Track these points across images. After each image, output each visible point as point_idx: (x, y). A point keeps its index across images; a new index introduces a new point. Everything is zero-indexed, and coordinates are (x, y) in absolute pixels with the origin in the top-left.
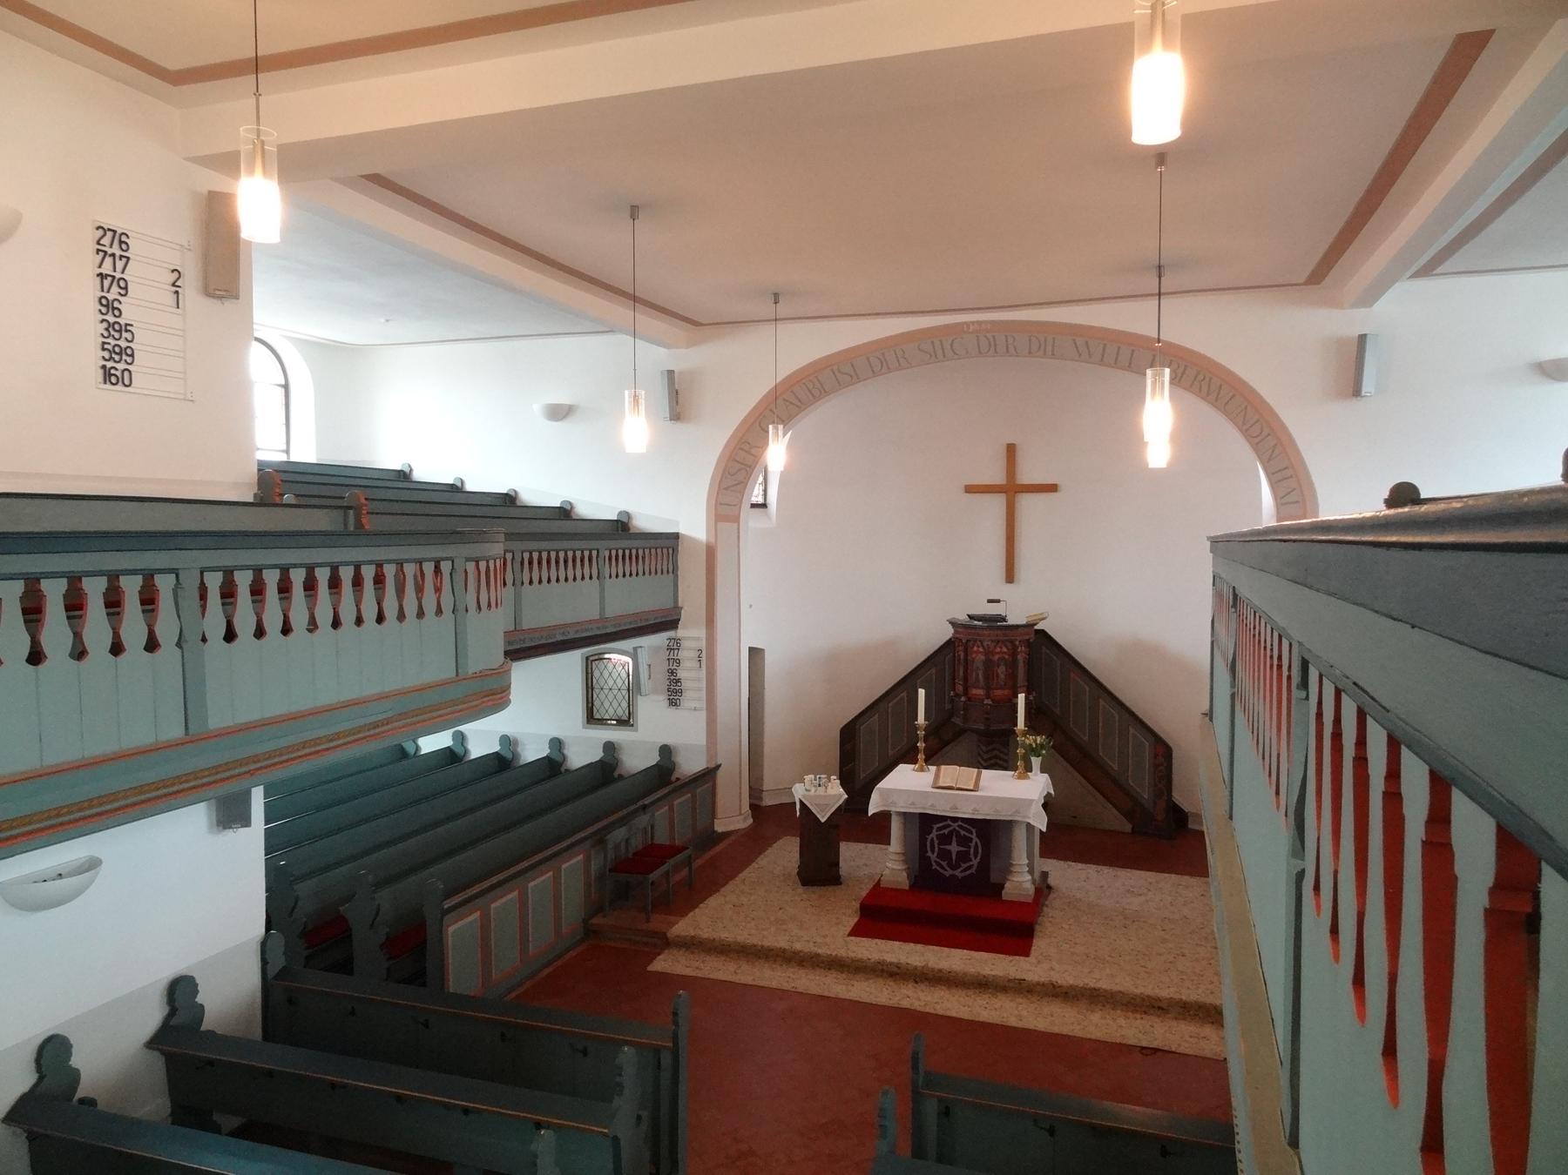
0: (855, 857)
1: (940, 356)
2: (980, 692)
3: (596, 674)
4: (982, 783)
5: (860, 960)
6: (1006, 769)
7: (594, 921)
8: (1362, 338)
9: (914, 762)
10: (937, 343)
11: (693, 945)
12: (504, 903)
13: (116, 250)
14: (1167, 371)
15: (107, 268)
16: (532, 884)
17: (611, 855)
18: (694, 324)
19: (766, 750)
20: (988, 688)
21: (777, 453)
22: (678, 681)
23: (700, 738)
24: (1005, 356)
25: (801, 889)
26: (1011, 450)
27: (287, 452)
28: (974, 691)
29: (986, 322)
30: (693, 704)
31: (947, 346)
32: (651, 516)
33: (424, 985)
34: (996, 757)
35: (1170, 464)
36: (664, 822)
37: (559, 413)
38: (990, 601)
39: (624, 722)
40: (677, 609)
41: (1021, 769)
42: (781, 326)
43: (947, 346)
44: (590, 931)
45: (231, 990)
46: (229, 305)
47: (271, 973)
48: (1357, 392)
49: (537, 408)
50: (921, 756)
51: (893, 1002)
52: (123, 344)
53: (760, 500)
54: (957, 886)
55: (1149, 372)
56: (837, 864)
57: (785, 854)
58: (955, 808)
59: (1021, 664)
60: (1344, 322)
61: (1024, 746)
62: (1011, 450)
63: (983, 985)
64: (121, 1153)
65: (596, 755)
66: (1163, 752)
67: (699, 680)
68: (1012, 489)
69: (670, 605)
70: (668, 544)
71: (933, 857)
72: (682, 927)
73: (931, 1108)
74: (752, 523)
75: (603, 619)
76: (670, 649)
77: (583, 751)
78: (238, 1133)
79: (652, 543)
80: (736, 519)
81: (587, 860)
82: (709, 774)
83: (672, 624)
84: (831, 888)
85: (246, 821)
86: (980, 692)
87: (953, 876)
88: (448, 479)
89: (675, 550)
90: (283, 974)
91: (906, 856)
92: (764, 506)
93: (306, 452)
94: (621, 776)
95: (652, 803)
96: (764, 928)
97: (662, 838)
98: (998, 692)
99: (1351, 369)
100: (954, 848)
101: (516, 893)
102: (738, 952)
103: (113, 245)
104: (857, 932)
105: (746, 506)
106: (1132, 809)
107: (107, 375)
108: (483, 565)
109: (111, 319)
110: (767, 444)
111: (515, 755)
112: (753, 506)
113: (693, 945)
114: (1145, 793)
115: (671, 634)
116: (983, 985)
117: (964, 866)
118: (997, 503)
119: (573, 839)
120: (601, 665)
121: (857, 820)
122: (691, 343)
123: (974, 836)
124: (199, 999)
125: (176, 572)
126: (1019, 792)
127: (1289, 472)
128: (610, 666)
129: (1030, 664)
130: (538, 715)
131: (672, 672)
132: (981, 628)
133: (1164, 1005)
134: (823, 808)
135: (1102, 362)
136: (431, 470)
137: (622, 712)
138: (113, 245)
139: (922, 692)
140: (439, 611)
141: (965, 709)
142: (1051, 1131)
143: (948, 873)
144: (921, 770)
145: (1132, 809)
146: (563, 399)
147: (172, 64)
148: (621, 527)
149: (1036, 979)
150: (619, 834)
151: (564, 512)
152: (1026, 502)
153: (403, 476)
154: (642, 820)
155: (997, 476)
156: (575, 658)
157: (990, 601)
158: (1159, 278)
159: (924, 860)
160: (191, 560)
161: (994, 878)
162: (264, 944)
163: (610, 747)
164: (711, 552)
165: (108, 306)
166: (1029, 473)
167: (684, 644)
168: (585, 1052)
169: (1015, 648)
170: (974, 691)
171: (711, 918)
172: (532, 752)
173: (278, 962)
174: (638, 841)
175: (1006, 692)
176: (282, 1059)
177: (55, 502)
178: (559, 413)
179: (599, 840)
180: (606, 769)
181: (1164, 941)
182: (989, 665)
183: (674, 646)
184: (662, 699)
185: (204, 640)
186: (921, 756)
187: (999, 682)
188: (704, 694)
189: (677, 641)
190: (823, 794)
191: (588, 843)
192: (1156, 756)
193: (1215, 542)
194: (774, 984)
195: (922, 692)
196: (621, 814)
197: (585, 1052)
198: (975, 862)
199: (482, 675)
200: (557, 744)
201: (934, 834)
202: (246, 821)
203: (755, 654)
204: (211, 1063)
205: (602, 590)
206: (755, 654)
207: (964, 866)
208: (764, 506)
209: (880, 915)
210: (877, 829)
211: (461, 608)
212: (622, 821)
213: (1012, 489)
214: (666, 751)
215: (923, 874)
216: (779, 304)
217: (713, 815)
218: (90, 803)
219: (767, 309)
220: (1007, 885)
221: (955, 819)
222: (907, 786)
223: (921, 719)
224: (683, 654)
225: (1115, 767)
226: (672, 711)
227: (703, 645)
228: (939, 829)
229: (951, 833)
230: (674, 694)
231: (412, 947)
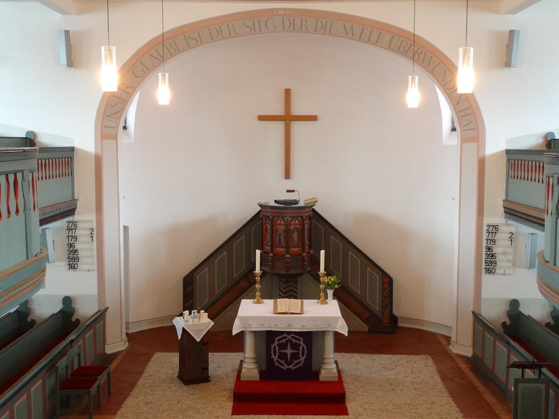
0: (221, 363)
2: (282, 250)
8: (512, 32)
9: (253, 297)
19: (107, 290)
20: (288, 247)
22: (76, 251)
23: (94, 291)
25: (185, 388)
26: (288, 92)
29: (289, 9)
30: (86, 267)
34: (291, 290)
35: (172, 102)
38: (288, 191)
41: (322, 298)
48: (508, 64)
50: (258, 294)
56: (207, 368)
57: (167, 363)
58: (290, 326)
59: (306, 231)
60: (503, 22)
61: (324, 283)
62: (288, 92)
66: (387, 281)
67: (91, 250)
68: (288, 118)
70: (63, 159)
71: (276, 358)
74: (124, 140)
76: (69, 229)
80: (115, 138)
81: (44, 384)
83: (71, 212)
84: (204, 385)
86: (282, 250)
87: (288, 369)
89: (514, 33)
91: (257, 360)
98: (293, 250)
100: (289, 351)
106: (370, 318)
110: (407, 88)
115: (70, 219)
117: (296, 362)
121: (224, 339)
122: (79, 13)
123: (302, 343)
126: (323, 313)
127: (468, 112)
129: (310, 230)
131: (71, 245)
132: (282, 208)
135: (360, 39)
141: (272, 262)
143: (285, 367)
145: (370, 318)
150: (62, 363)
152: (296, 126)
155: (279, 111)
157: (288, 191)
159: (270, 361)
161: (314, 369)
164: (98, 160)
166: (296, 110)
169: (303, 220)
181: (419, 396)
182: (288, 232)
183: (72, 227)
184: (63, 265)
186: (258, 294)
187: (288, 244)
189: (74, 223)
192: (383, 283)
193: (260, 205)
198: (302, 359)
201: (276, 343)
203: (126, 228)
206: (126, 228)
207: (296, 362)
210: (236, 343)
213: (288, 118)
214: (67, 301)
215: (269, 371)
220: (323, 371)
221: (289, 333)
222: (255, 313)
223: (258, 270)
225: (359, 292)
226: (72, 273)
227: (94, 226)
228: (279, 340)
229: (287, 342)
230: (73, 260)
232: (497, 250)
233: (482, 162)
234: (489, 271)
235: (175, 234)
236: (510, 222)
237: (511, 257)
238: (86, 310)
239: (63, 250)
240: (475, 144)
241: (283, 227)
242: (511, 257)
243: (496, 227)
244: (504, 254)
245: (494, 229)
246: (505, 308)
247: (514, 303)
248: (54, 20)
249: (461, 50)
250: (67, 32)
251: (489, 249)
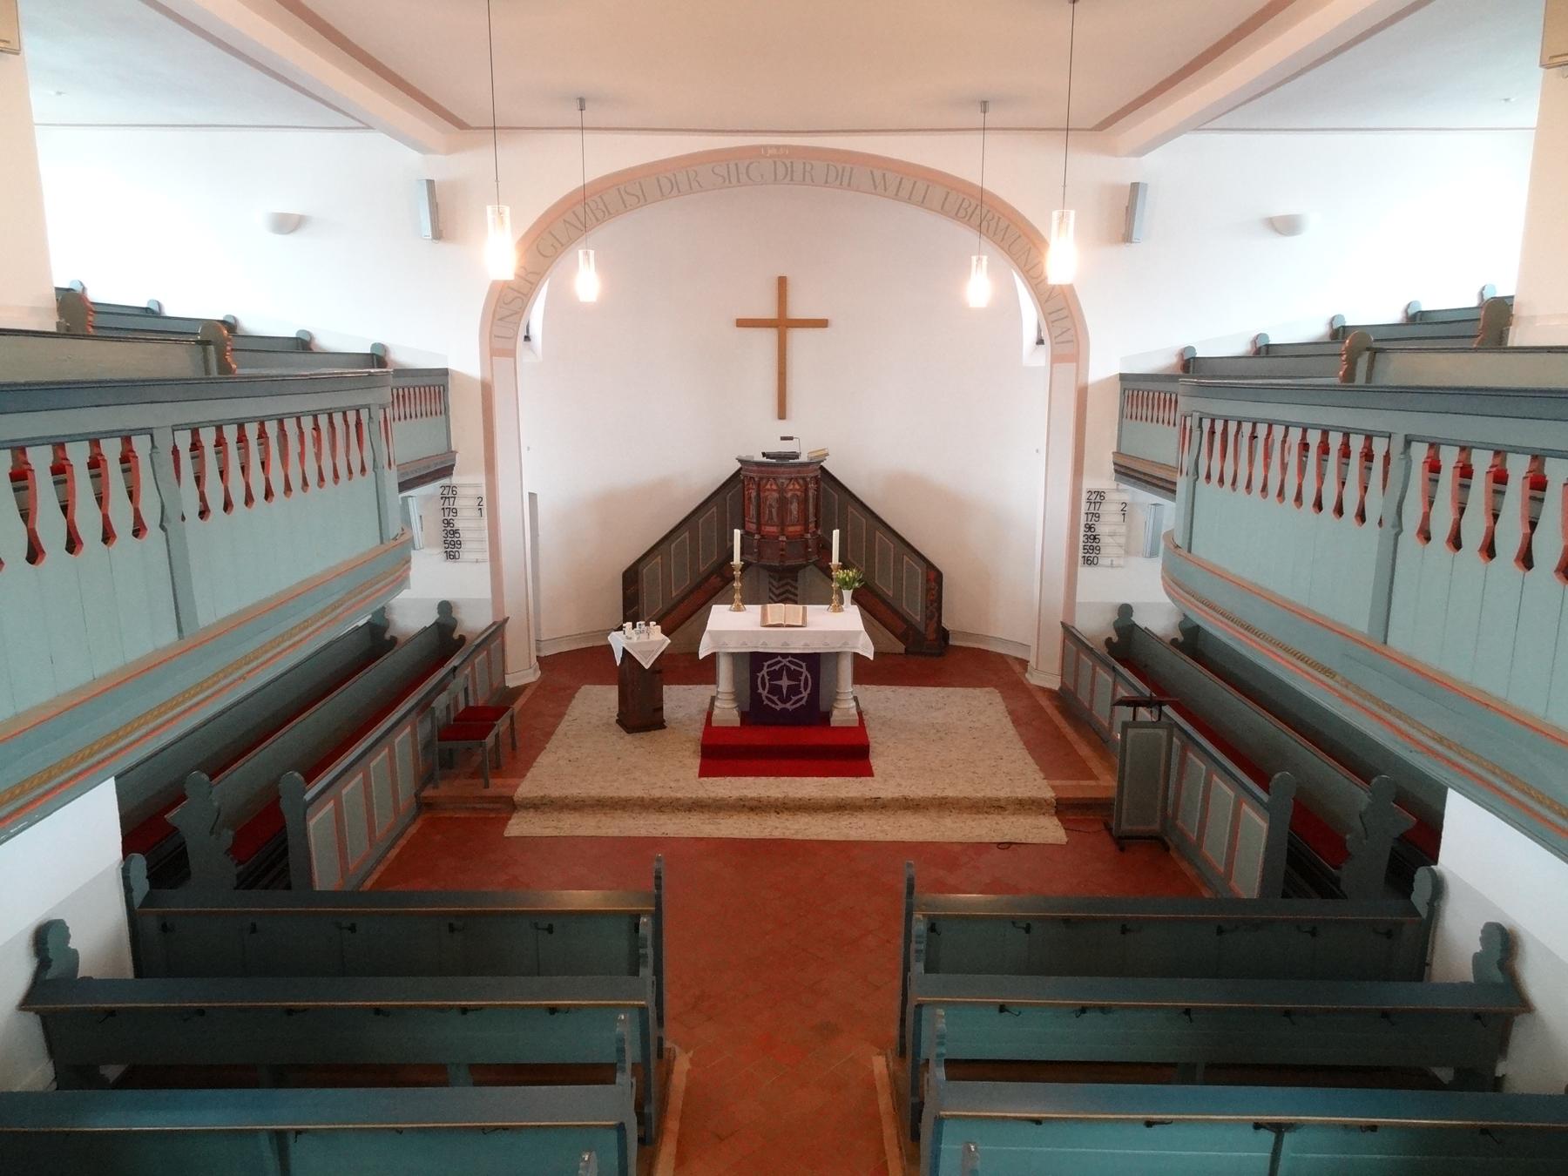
0: (682, 702)
1: (734, 180)
2: (774, 529)
4: (809, 619)
5: (722, 799)
6: (796, 603)
7: (424, 794)
8: (1135, 187)
10: (732, 167)
11: (541, 805)
14: (1072, 213)
22: (455, 532)
23: (484, 591)
24: (789, 186)
25: (628, 737)
26: (782, 282)
28: (768, 529)
29: (785, 147)
30: (473, 556)
31: (742, 170)
32: (413, 348)
33: (288, 887)
36: (460, 687)
37: (288, 224)
38: (783, 439)
40: (451, 453)
42: (989, 136)
43: (742, 170)
44: (423, 805)
45: (99, 931)
47: (138, 897)
48: (1127, 238)
50: (737, 596)
51: (766, 834)
54: (788, 720)
57: (599, 701)
60: (1126, 169)
61: (838, 580)
62: (782, 282)
63: (841, 807)
64: (68, 1134)
66: (934, 577)
68: (782, 324)
70: (431, 387)
71: (765, 693)
72: (526, 789)
73: (919, 927)
74: (527, 358)
76: (444, 498)
78: (123, 1083)
80: (512, 353)
81: (414, 733)
82: (498, 629)
83: (446, 471)
86: (774, 529)
88: (142, 302)
90: (148, 901)
91: (736, 696)
96: (595, 782)
98: (791, 529)
99: (1125, 216)
100: (785, 683)
102: (592, 806)
104: (705, 772)
113: (541, 805)
114: (917, 615)
116: (841, 807)
117: (794, 699)
122: (451, 150)
123: (804, 670)
124: (72, 945)
125: (148, 431)
126: (836, 624)
129: (817, 499)
133: (1003, 804)
134: (646, 654)
135: (896, 197)
142: (1028, 929)
144: (738, 609)
146: (293, 208)
149: (890, 796)
150: (441, 701)
151: (302, 345)
152: (797, 337)
155: (770, 312)
157: (783, 439)
158: (984, 112)
159: (755, 697)
161: (823, 708)
164: (487, 390)
166: (796, 311)
168: (550, 930)
169: (806, 484)
170: (768, 529)
171: (539, 779)
174: (441, 704)
175: (798, 528)
176: (157, 996)
177: (1545, 356)
178: (288, 224)
182: (783, 502)
183: (449, 494)
184: (437, 553)
185: (183, 518)
186: (737, 596)
187: (783, 520)
188: (486, 545)
189: (452, 488)
190: (644, 641)
191: (414, 713)
192: (928, 580)
194: (643, 833)
197: (550, 930)
198: (805, 694)
203: (532, 496)
204: (111, 1013)
206: (532, 496)
207: (794, 699)
209: (720, 754)
210: (704, 671)
213: (782, 324)
214: (445, 607)
215: (754, 712)
216: (583, 111)
217: (504, 672)
219: (573, 116)
220: (835, 712)
221: (785, 656)
222: (732, 625)
223: (737, 560)
224: (459, 503)
226: (450, 564)
227: (483, 492)
230: (452, 545)
231: (267, 846)
232: (1102, 529)
233: (1082, 394)
234: (1088, 561)
235: (608, 505)
236: (1123, 486)
237: (1122, 540)
238: (474, 621)
239: (437, 531)
242: (1122, 540)
243: (1100, 494)
244: (1112, 535)
245: (1098, 497)
246: (1112, 617)
247: (1125, 610)
249: (1055, 214)
250: (430, 183)
251: (1090, 528)
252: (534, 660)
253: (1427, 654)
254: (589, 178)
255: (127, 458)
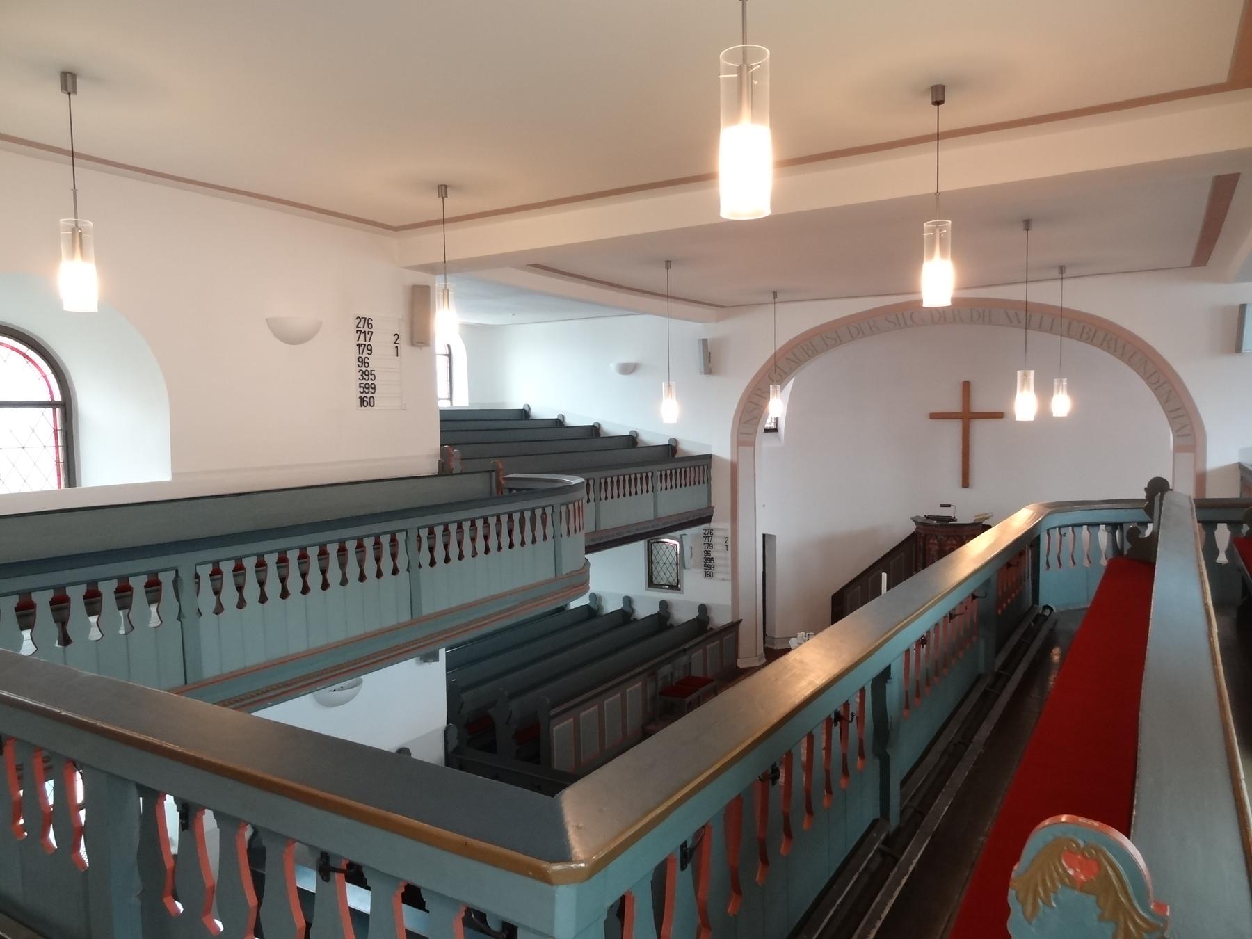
3: (655, 552)
12: (588, 713)
13: (366, 329)
14: (1032, 372)
15: (362, 341)
16: (582, 714)
17: (660, 683)
18: (721, 308)
21: (777, 407)
23: (727, 601)
26: (966, 386)
27: (451, 399)
30: (721, 576)
32: (693, 442)
33: (539, 763)
36: (698, 661)
37: (628, 369)
39: (675, 587)
40: (710, 508)
46: (425, 349)
47: (450, 749)
48: (1238, 349)
49: (613, 366)
52: (370, 382)
53: (773, 426)
55: (1019, 373)
62: (966, 386)
65: (655, 609)
68: (967, 416)
69: (704, 505)
70: (704, 462)
74: (765, 444)
75: (656, 519)
77: (646, 606)
79: (693, 463)
80: (753, 444)
82: (734, 627)
83: (708, 519)
85: (436, 659)
89: (709, 467)
90: (457, 750)
92: (776, 430)
93: (462, 401)
94: (672, 626)
95: (691, 647)
97: (697, 672)
101: (619, 695)
103: (364, 326)
105: (760, 430)
107: (362, 401)
108: (571, 506)
109: (364, 369)
111: (600, 608)
112: (766, 431)
118: (956, 427)
119: (633, 673)
120: (658, 546)
122: (719, 319)
125: (406, 530)
128: (664, 547)
130: (615, 580)
131: (707, 553)
136: (543, 409)
137: (672, 579)
138: (364, 326)
139: (884, 575)
140: (545, 538)
147: (395, 224)
148: (671, 449)
150: (666, 670)
153: (524, 414)
154: (684, 659)
155: (956, 407)
156: (639, 547)
160: (412, 523)
162: (446, 732)
163: (664, 604)
164: (734, 468)
165: (363, 362)
167: (716, 533)
172: (612, 605)
173: (454, 743)
178: (628, 369)
179: (652, 673)
180: (662, 618)
183: (708, 535)
184: (700, 572)
188: (729, 569)
189: (711, 530)
195: (884, 575)
196: (668, 655)
199: (570, 575)
200: (628, 600)
202: (436, 659)
205: (655, 497)
208: (776, 430)
211: (558, 535)
212: (668, 661)
213: (967, 416)
214: (703, 609)
217: (736, 656)
218: (368, 657)
224: (714, 540)
226: (707, 581)
227: (729, 535)
230: (709, 568)
235: (829, 546)
238: (720, 619)
239: (700, 556)
240: (1192, 455)
241: (936, 548)
248: (689, 330)
250: (705, 341)
252: (761, 651)
253: (442, 605)
254: (781, 343)
255: (393, 541)
